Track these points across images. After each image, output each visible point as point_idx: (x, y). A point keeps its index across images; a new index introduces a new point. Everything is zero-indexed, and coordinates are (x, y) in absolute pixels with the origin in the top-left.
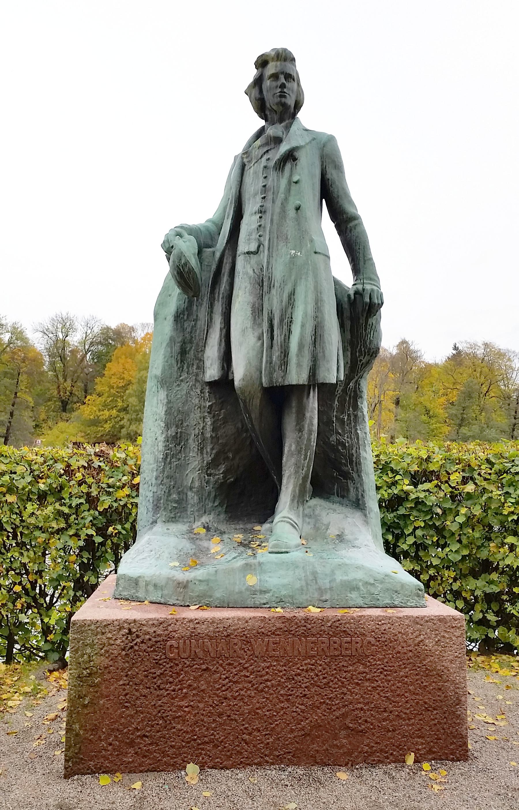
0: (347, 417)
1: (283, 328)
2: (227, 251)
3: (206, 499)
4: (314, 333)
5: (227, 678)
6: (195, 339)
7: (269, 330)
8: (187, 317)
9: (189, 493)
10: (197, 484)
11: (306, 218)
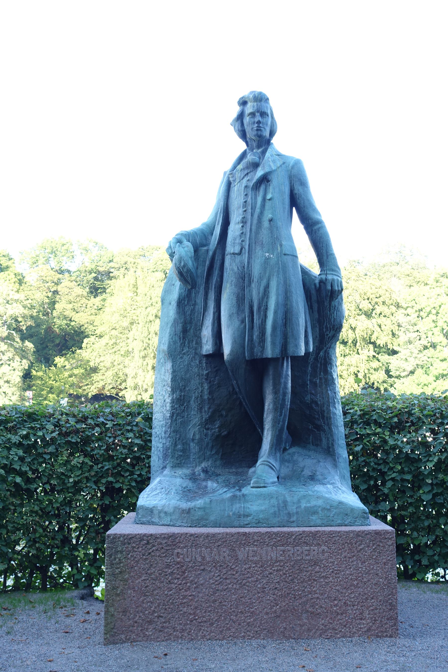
2: (218, 250)
3: (205, 449)
4: (284, 317)
5: (219, 576)
7: (250, 315)
8: (188, 302)
9: (192, 444)
10: (197, 437)
11: (277, 227)
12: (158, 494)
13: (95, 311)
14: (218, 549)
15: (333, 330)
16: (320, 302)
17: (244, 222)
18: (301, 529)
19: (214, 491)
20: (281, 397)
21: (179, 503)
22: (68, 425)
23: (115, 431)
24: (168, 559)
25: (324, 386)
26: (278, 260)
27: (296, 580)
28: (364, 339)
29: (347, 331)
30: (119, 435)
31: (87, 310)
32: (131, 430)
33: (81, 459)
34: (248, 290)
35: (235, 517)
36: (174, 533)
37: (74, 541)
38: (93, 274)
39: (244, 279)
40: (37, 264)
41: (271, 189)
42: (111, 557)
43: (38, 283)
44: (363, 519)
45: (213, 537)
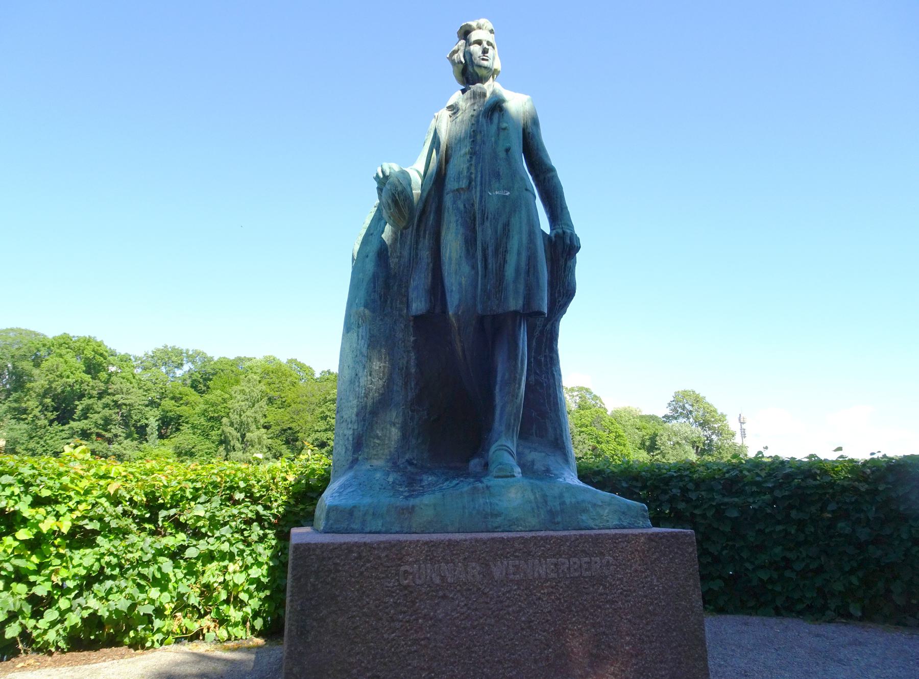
21: (392, 499)
24: (389, 582)
27: (573, 608)
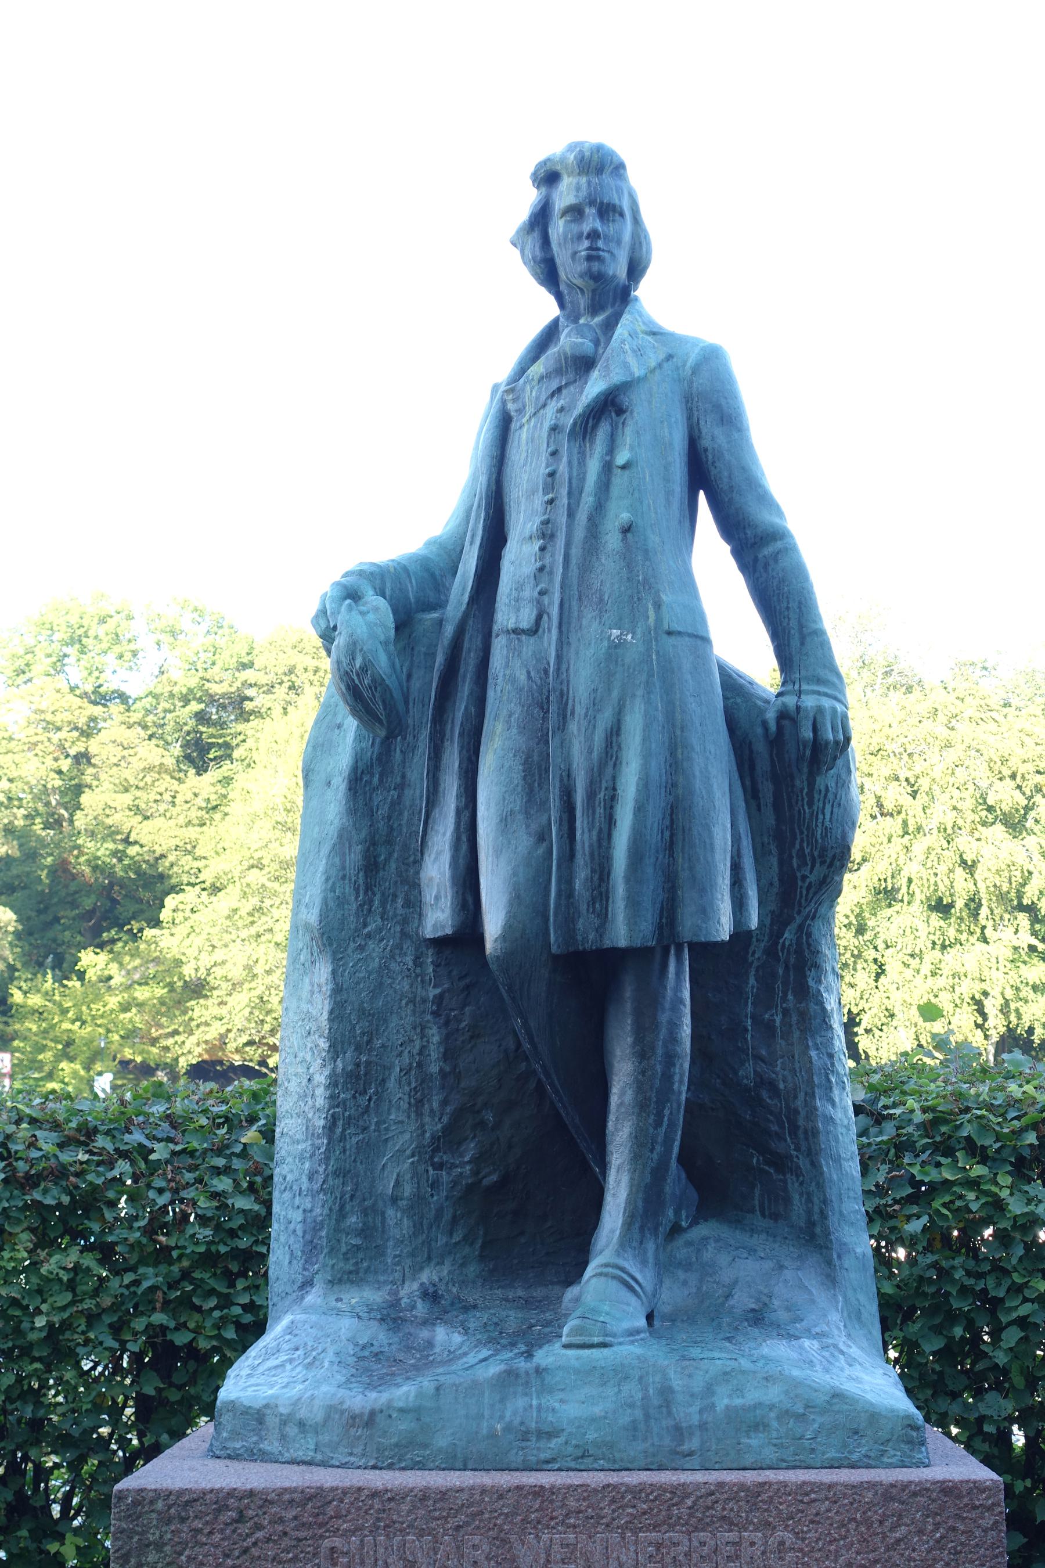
0: (780, 1016)
1: (594, 812)
2: (471, 622)
3: (430, 1227)
4: (667, 822)
6: (401, 833)
7: (565, 817)
8: (381, 780)
9: (390, 1212)
10: (408, 1190)
11: (646, 551)
12: (282, 1366)
13: (200, 813)
14: (455, 1539)
15: (823, 863)
16: (781, 778)
17: (546, 534)
18: (713, 1477)
19: (452, 1356)
20: (659, 1068)
21: (342, 1392)
22: (34, 1154)
23: (177, 1170)
25: (797, 1034)
26: (649, 650)
28: (1002, 897)
29: (951, 871)
30: (188, 1185)
31: (174, 811)
32: (227, 1171)
33: (72, 1257)
34: (557, 739)
35: (512, 1437)
36: (321, 1488)
37: (56, 1510)
38: (193, 703)
39: (548, 706)
40: (28, 676)
41: (628, 436)
42: (127, 1562)
43: (31, 731)
44: (905, 1448)
45: (441, 1500)
